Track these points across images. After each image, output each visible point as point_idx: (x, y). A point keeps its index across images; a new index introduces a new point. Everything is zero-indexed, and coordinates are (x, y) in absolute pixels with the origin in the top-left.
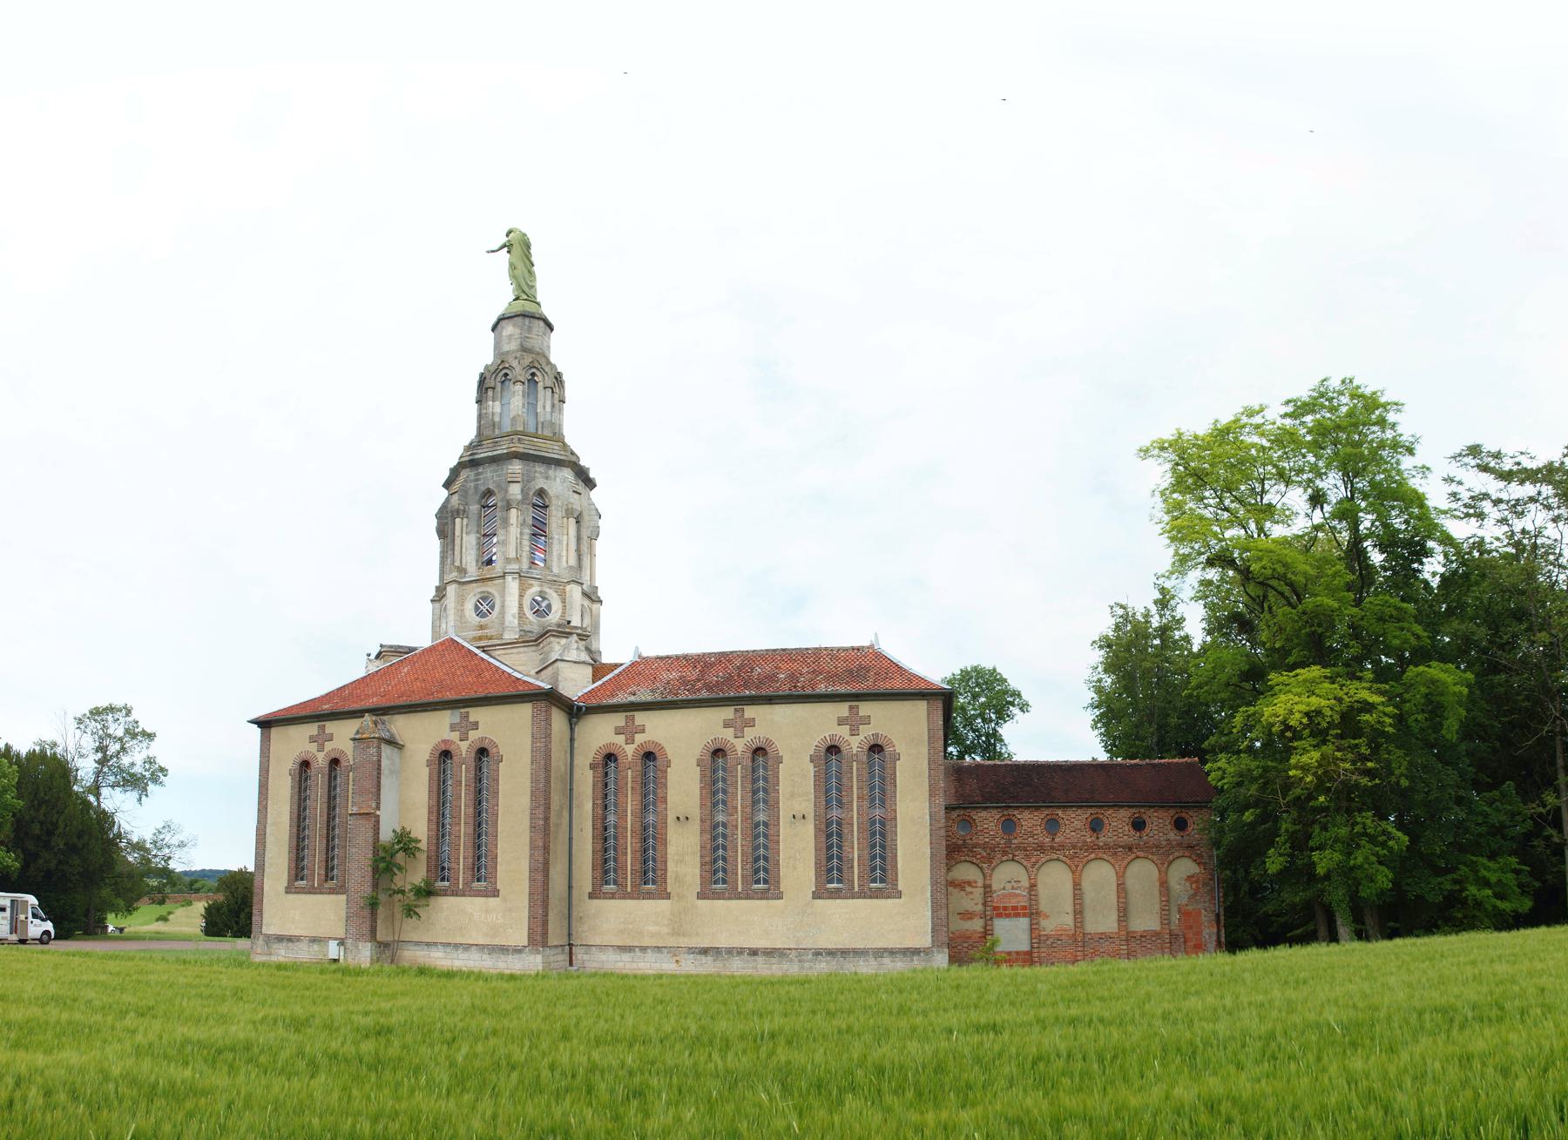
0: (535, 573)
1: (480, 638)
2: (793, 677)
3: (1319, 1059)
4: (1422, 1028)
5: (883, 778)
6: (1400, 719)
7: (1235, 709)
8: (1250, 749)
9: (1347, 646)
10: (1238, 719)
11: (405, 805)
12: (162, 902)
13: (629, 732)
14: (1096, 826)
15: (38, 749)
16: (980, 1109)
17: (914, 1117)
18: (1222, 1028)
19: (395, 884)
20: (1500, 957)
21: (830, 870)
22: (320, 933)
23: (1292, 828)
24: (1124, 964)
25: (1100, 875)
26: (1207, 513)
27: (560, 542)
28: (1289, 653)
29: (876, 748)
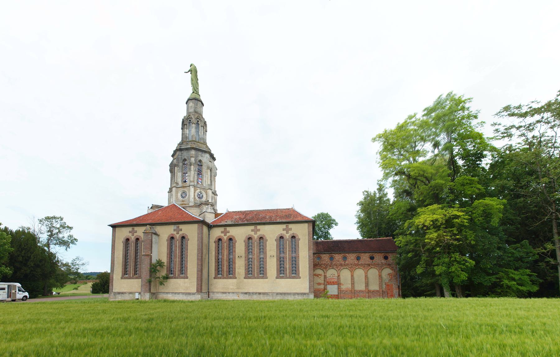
0: (199, 186)
1: (183, 204)
2: (270, 217)
3: (437, 337)
4: (481, 331)
5: (295, 245)
6: (471, 220)
7: (405, 221)
8: (410, 234)
9: (448, 196)
10: (406, 224)
11: (160, 252)
12: (75, 283)
13: (225, 233)
14: (358, 258)
15: (21, 230)
16: (323, 341)
17: (304, 342)
18: (400, 322)
19: (155, 277)
20: (520, 308)
21: (281, 271)
22: (133, 291)
23: (426, 259)
24: (367, 300)
25: (360, 273)
26: (395, 157)
28: (425, 201)
29: (293, 237)
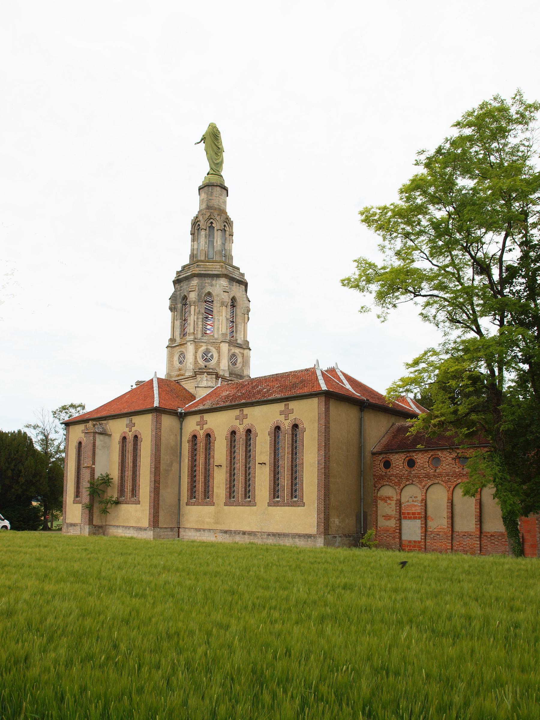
27: (219, 320)
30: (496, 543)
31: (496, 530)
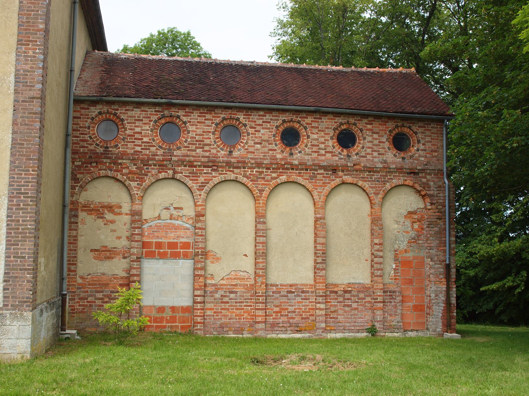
25: (292, 206)
30: (354, 305)
31: (352, 281)
